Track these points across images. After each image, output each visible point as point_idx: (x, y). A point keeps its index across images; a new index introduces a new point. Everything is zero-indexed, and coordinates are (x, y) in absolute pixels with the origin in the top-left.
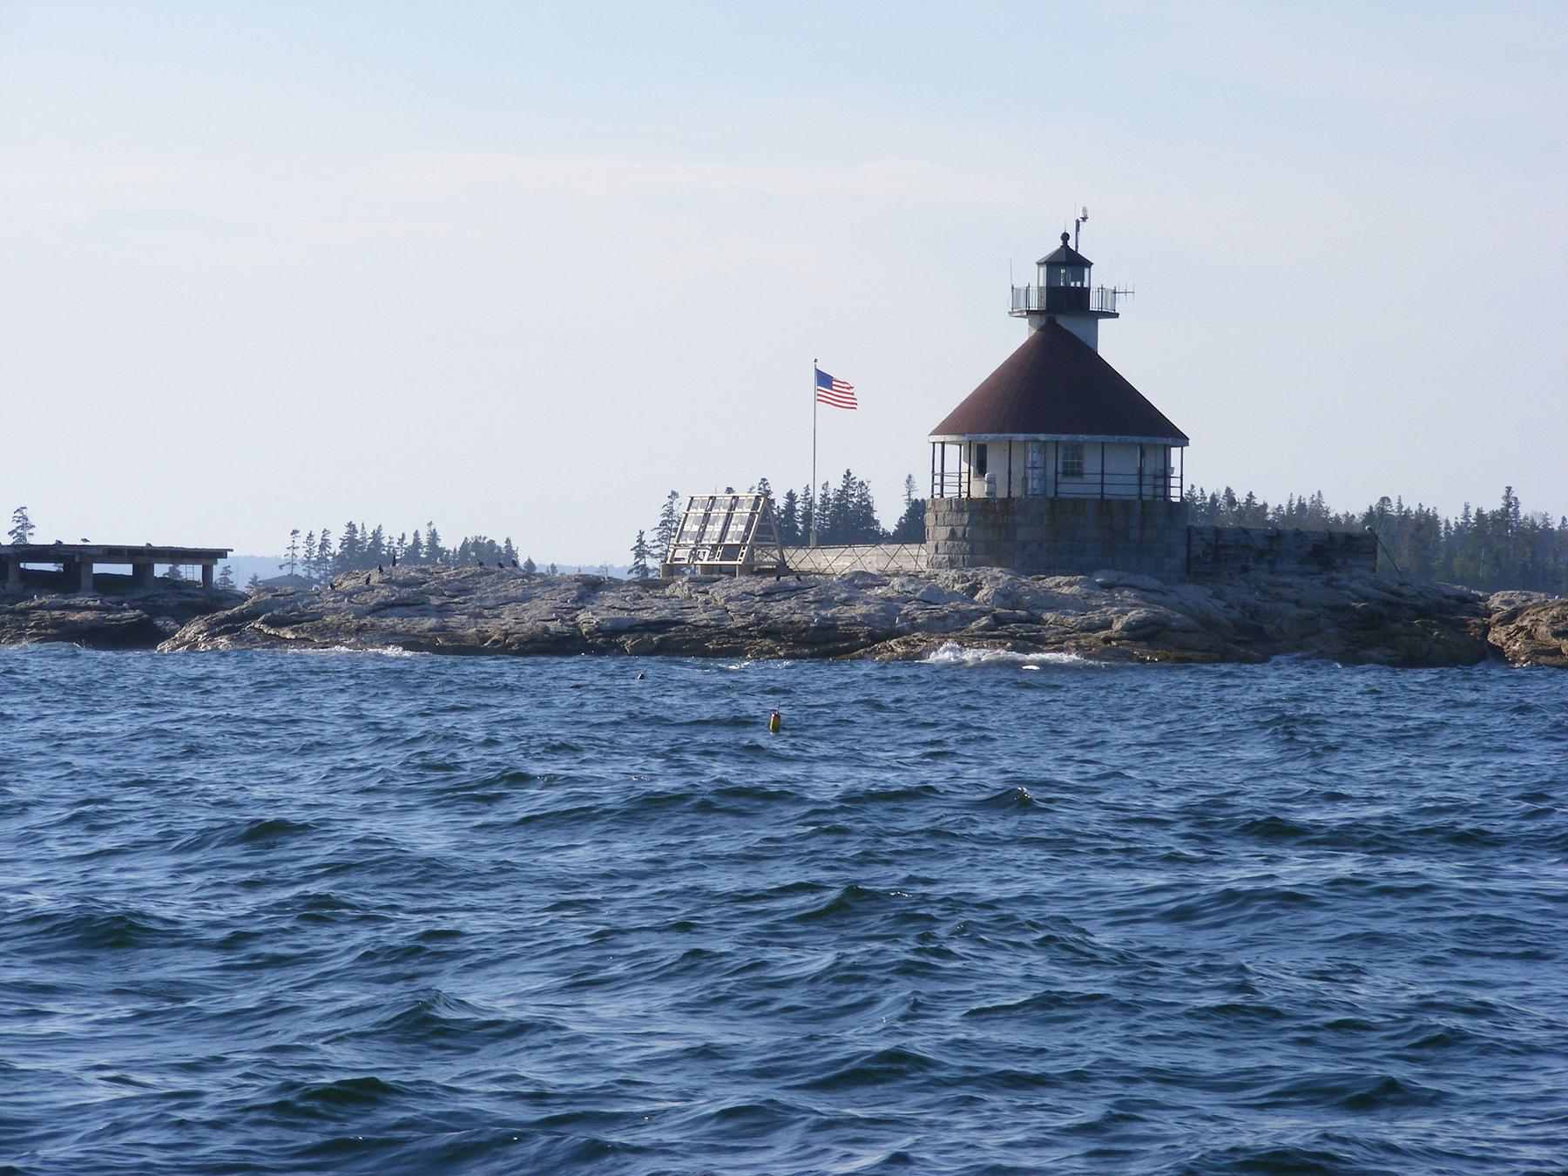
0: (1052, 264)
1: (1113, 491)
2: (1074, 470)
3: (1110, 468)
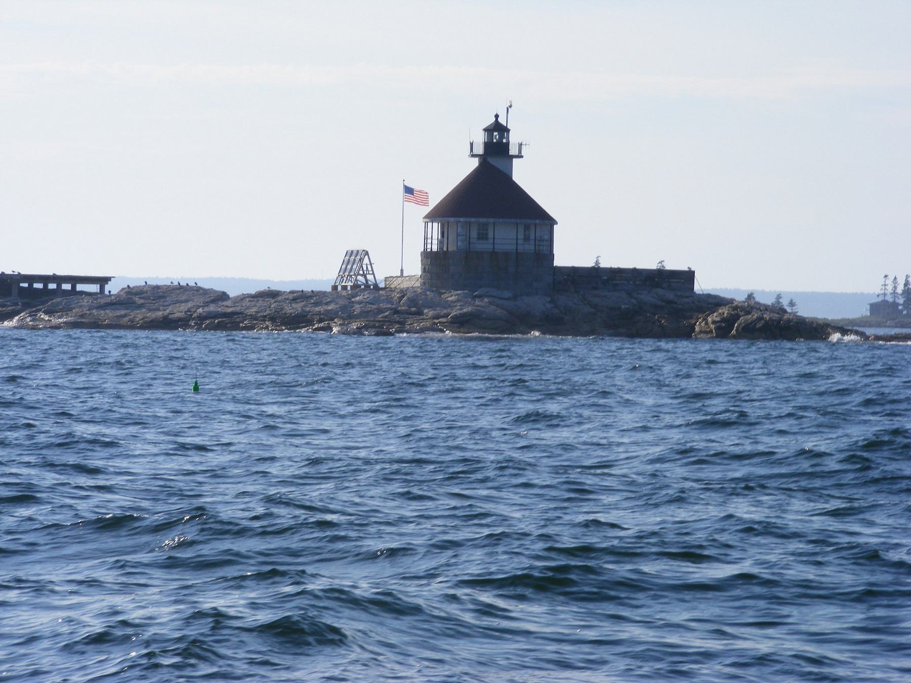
0: (489, 130)
1: (498, 248)
2: (483, 236)
3: (505, 236)
